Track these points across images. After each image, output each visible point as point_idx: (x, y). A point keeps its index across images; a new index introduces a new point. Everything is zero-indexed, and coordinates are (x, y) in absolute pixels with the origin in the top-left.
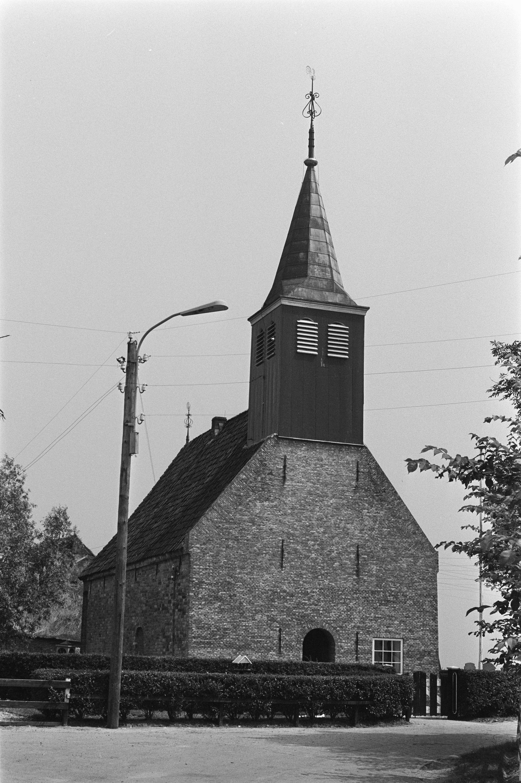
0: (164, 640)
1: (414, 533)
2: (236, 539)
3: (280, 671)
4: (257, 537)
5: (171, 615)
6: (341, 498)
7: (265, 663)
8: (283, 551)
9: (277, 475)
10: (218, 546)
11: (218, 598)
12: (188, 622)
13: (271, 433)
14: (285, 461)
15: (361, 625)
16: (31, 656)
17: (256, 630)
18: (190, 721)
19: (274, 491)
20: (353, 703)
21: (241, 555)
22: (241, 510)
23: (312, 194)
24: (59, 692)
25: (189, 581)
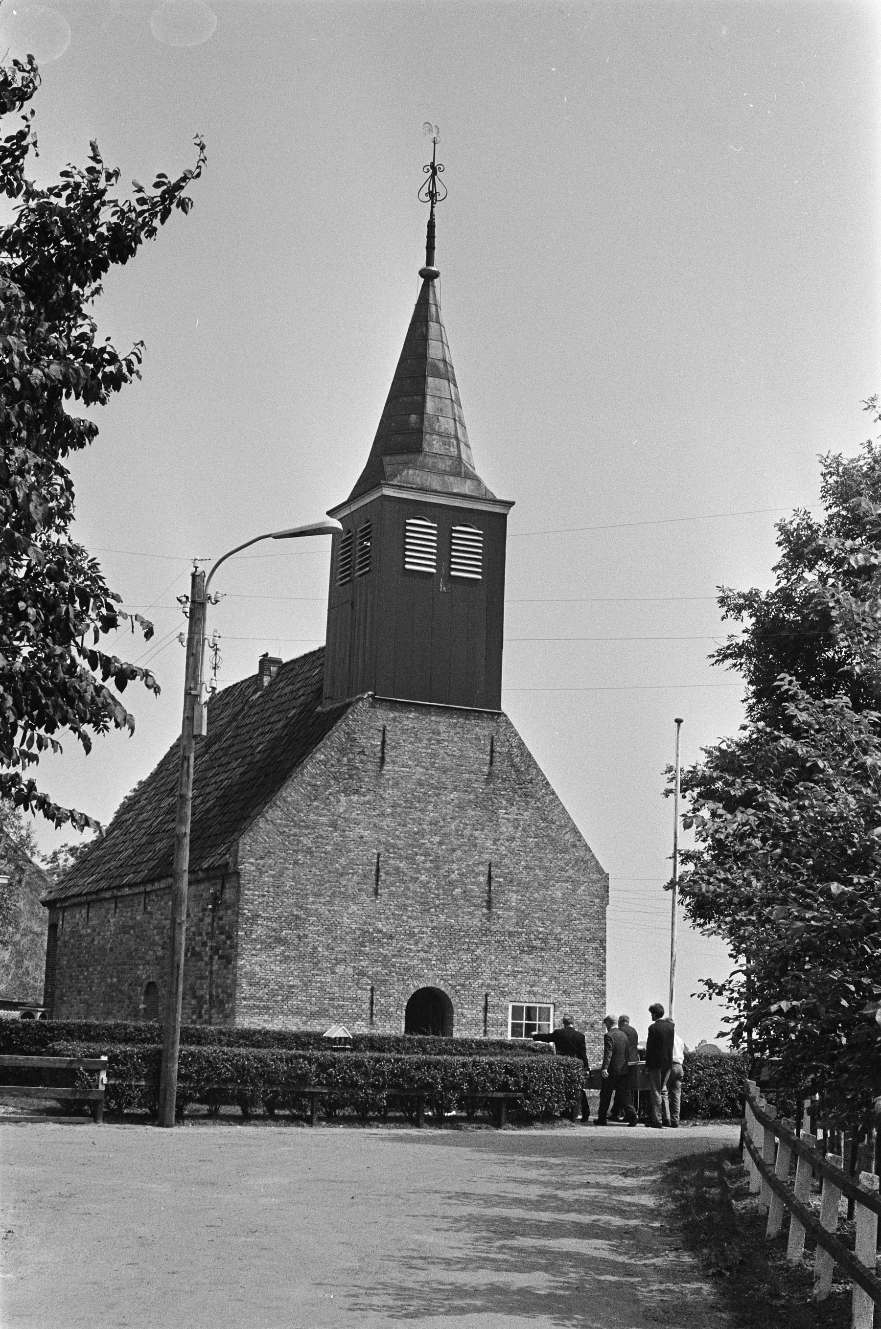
0: (193, 1002)
1: (574, 846)
2: (309, 852)
3: (388, 1049)
4: (340, 849)
5: (207, 964)
6: (466, 791)
7: (366, 1036)
8: (378, 870)
9: (372, 755)
10: (282, 861)
11: (280, 941)
12: (235, 975)
13: (364, 691)
14: (384, 734)
15: (494, 982)
16: (24, 1024)
17: (337, 989)
18: (270, 1117)
19: (366, 780)
20: (500, 1095)
21: (315, 875)
22: (317, 807)
23: (431, 323)
24: (91, 1075)
25: (237, 914)
